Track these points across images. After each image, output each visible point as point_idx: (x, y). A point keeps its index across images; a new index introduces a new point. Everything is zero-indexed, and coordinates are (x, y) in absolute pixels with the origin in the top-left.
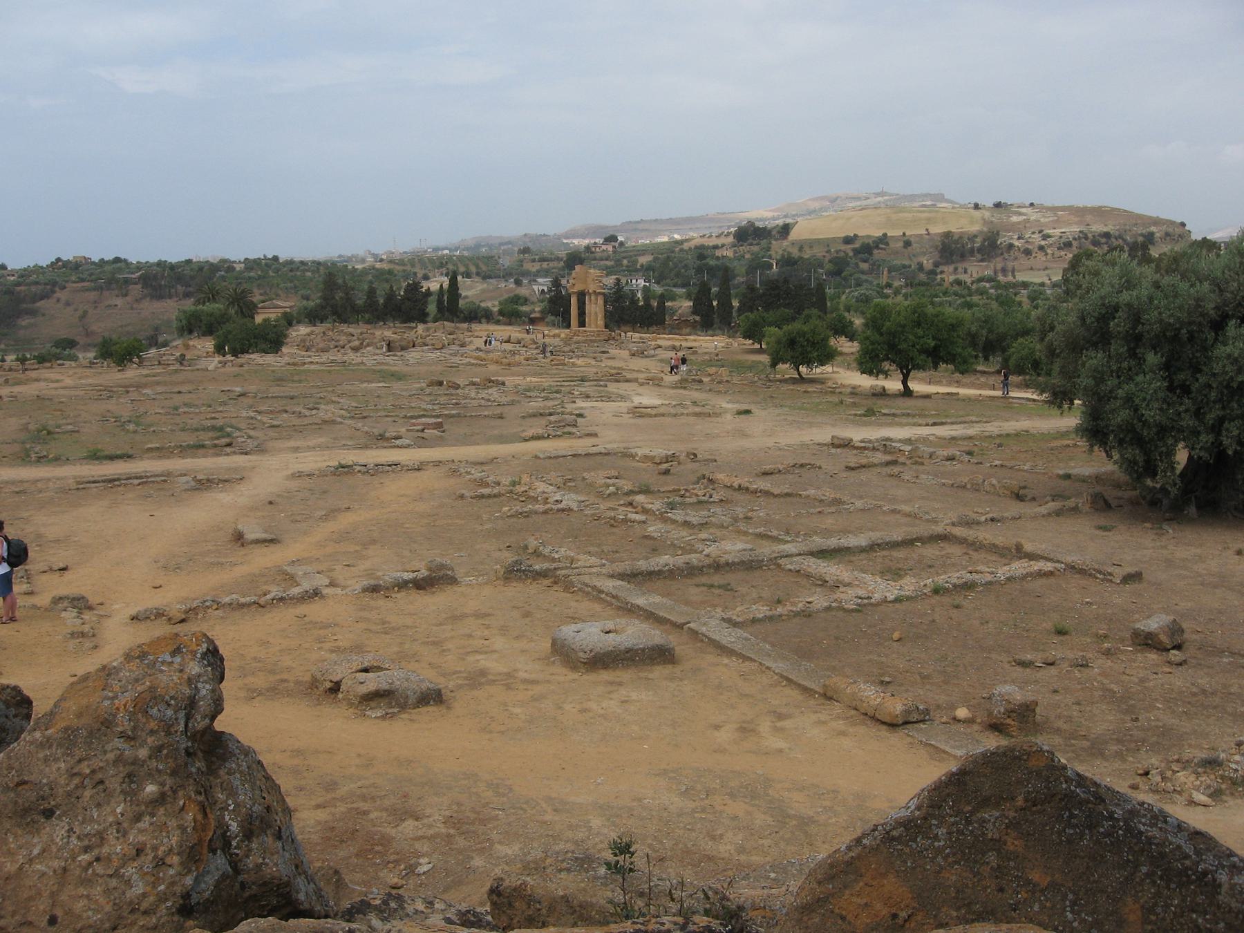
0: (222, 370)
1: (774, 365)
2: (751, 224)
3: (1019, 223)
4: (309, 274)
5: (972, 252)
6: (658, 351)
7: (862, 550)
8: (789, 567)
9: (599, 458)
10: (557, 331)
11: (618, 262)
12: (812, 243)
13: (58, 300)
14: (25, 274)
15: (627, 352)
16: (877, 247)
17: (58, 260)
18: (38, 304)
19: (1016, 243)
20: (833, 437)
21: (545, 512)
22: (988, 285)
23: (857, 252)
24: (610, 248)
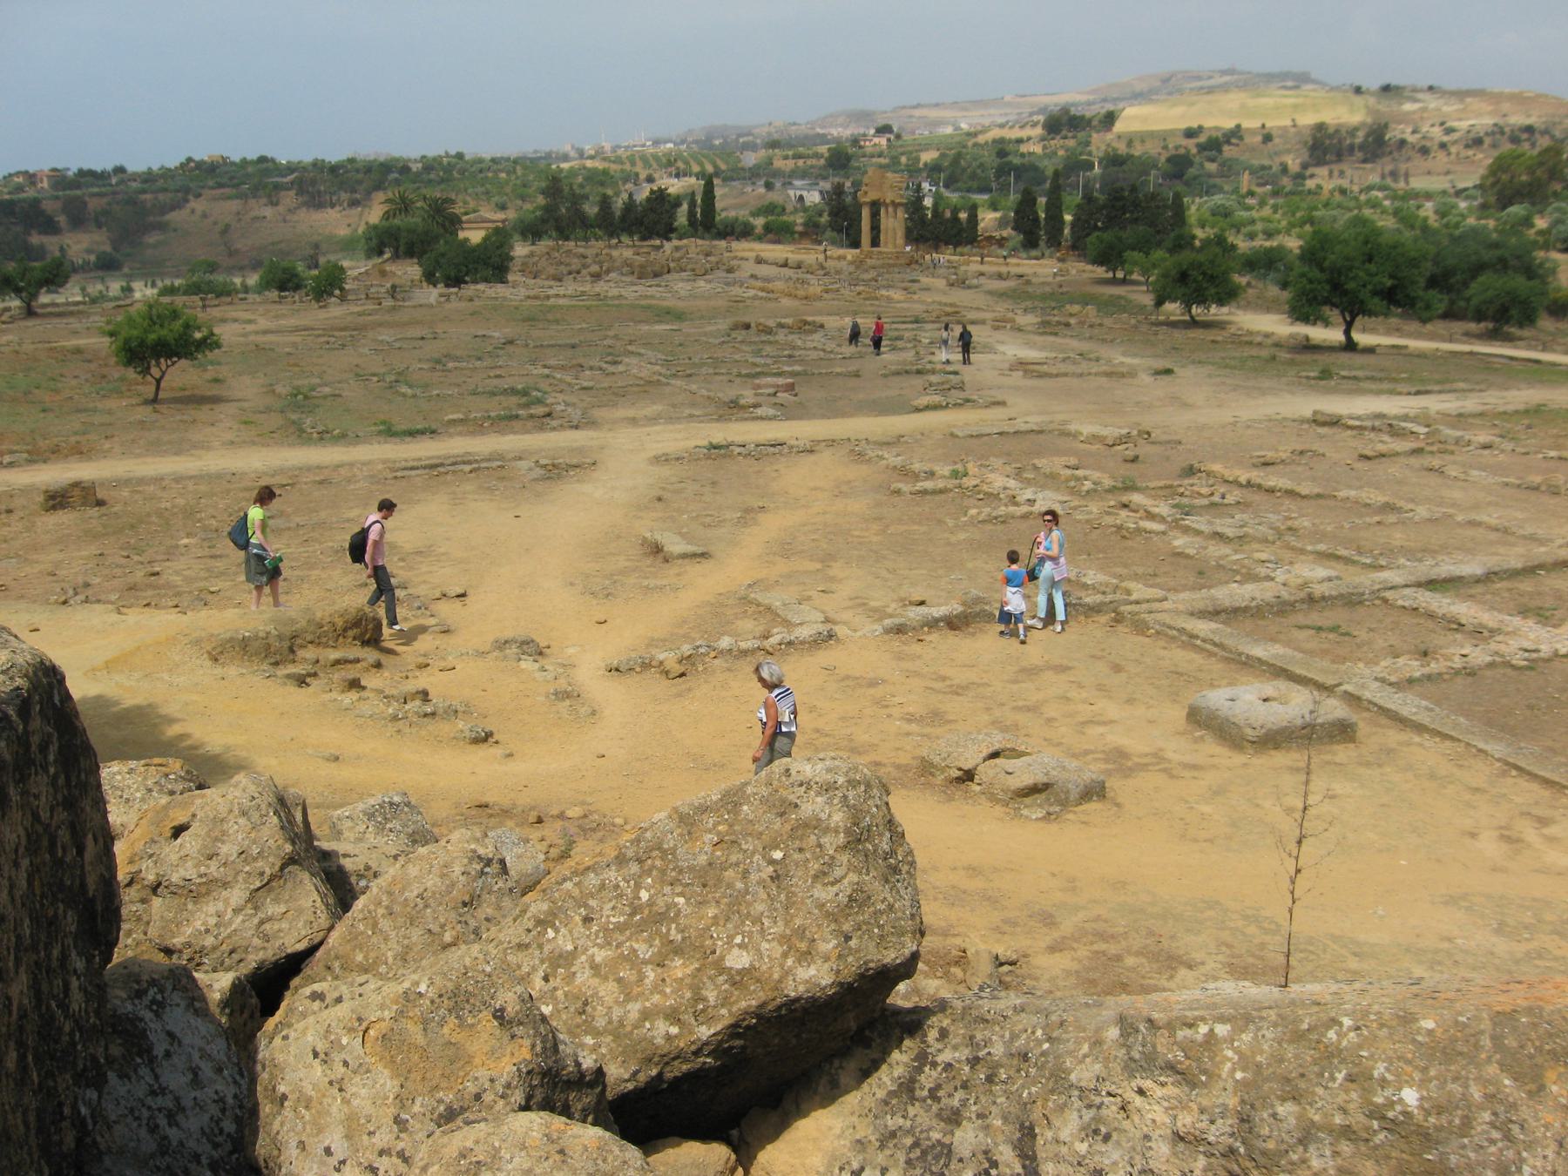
0: (448, 306)
1: (1159, 303)
2: (1065, 110)
3: (1414, 112)
4: (503, 175)
5: (1351, 148)
6: (982, 280)
7: (1478, 581)
8: (1400, 602)
9: (1032, 436)
10: (841, 252)
11: (895, 160)
12: (1144, 137)
13: (193, 211)
14: (149, 178)
15: (944, 282)
16: (1228, 142)
17: (190, 160)
18: (168, 217)
19: (1411, 139)
20: (1315, 413)
21: (1025, 517)
22: (1380, 194)
23: (1202, 148)
24: (883, 141)
